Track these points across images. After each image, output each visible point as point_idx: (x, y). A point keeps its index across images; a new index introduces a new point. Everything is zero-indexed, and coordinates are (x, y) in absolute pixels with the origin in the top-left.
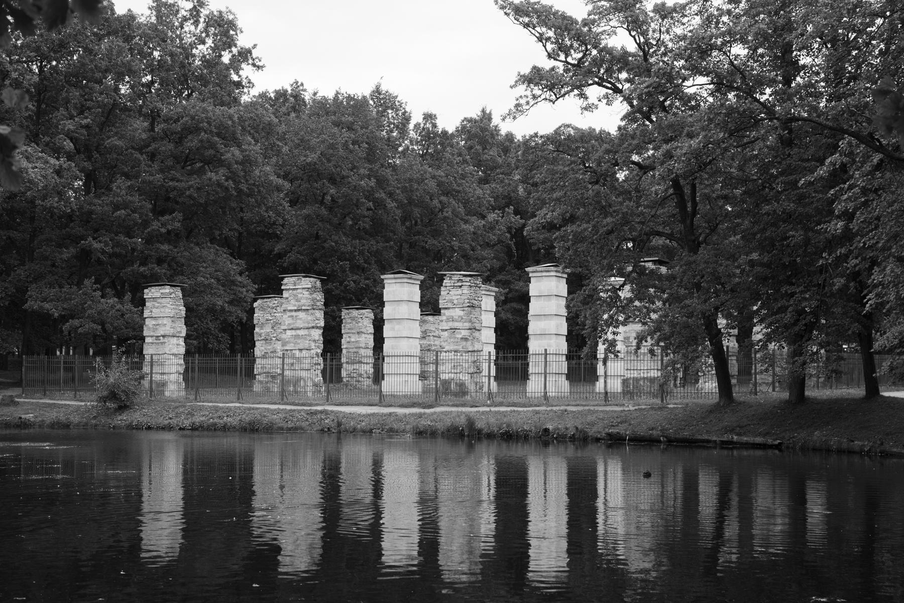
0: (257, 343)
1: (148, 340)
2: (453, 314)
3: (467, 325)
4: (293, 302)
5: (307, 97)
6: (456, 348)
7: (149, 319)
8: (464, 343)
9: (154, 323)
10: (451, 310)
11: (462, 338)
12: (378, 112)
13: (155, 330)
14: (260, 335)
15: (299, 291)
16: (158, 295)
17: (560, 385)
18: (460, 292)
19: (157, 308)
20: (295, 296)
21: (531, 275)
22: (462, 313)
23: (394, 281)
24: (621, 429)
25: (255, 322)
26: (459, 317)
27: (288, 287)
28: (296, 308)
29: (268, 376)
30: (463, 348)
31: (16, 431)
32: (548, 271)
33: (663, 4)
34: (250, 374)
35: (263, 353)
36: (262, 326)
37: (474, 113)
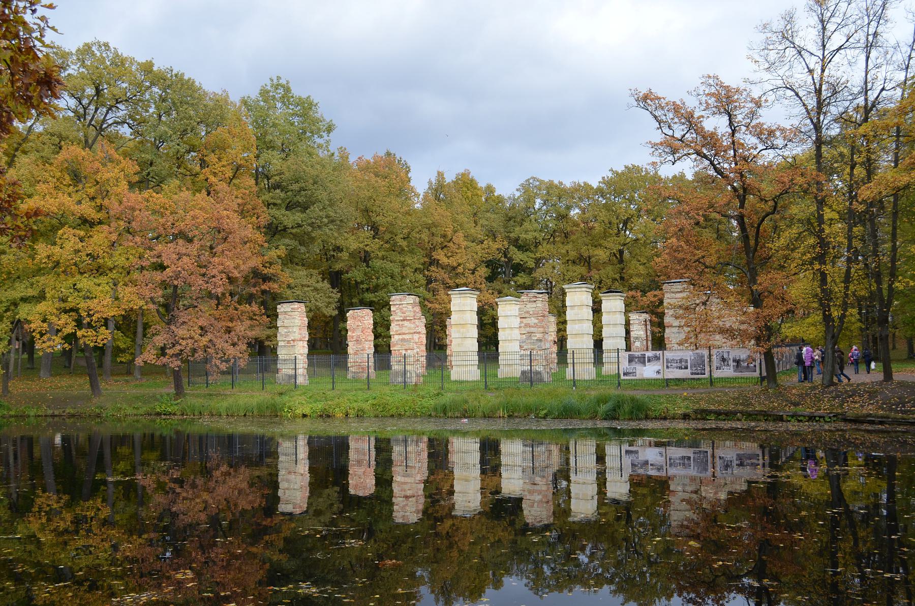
3: (541, 330)
4: (400, 314)
5: (352, 159)
13: (286, 336)
14: (352, 337)
16: (289, 310)
18: (534, 305)
22: (536, 321)
23: (459, 296)
31: (722, 424)
33: (183, 74)
37: (462, 171)
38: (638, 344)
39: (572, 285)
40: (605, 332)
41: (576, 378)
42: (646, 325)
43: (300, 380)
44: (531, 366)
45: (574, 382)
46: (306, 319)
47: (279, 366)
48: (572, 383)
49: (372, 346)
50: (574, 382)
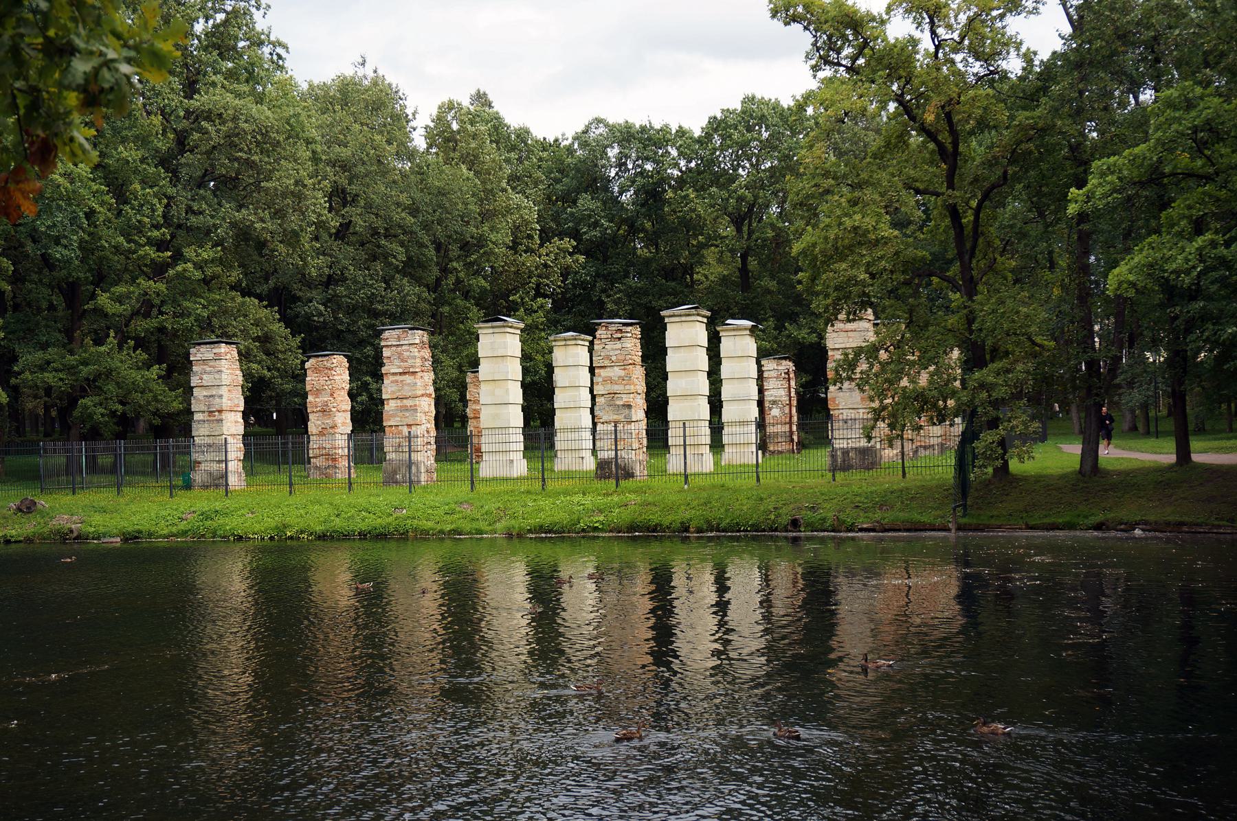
0: (311, 416)
1: (197, 417)
2: (611, 374)
4: (397, 362)
6: (615, 417)
7: (199, 389)
8: (627, 411)
9: (205, 394)
10: (609, 369)
11: (623, 405)
12: (923, 211)
15: (404, 347)
16: (211, 356)
17: (707, 462)
18: (619, 345)
19: (209, 373)
20: (400, 354)
21: (666, 320)
23: (491, 331)
24: (655, 517)
25: (308, 388)
26: (619, 377)
27: (390, 343)
28: (401, 371)
29: (328, 459)
30: (625, 417)
32: (689, 315)
34: (302, 458)
35: (320, 429)
36: (318, 392)
38: (775, 412)
39: (676, 310)
40: (726, 392)
41: (688, 471)
42: (789, 380)
43: (233, 480)
44: (616, 450)
45: (686, 477)
46: (239, 373)
47: (195, 456)
48: (683, 479)
49: (349, 421)
50: (686, 477)
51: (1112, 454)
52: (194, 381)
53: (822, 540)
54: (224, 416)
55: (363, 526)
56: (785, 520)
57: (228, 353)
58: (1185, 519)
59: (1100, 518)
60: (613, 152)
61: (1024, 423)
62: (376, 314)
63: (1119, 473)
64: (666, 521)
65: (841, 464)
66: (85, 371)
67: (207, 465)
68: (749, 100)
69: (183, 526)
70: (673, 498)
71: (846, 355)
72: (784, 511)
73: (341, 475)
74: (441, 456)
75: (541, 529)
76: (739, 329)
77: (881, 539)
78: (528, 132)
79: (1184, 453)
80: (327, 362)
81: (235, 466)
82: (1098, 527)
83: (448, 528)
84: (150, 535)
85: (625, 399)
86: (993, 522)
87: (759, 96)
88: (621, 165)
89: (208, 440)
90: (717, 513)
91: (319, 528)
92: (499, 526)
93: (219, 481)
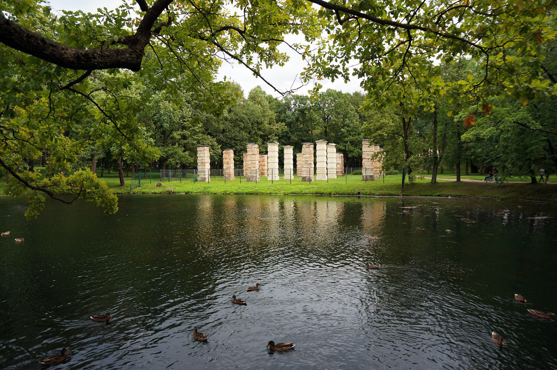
1: (198, 164)
4: (251, 152)
16: (202, 149)
18: (308, 149)
36: (226, 159)
39: (319, 141)
51: (440, 179)
52: (198, 155)
53: (366, 197)
54: (206, 164)
55: (247, 191)
56: (356, 192)
57: (207, 149)
58: (462, 194)
59: (439, 194)
60: (292, 102)
61: (422, 171)
62: (236, 140)
63: (442, 183)
64: (325, 192)
65: (366, 179)
66: (170, 152)
67: (201, 176)
68: (329, 89)
69: (200, 190)
70: (326, 186)
71: (375, 153)
72: (356, 190)
73: (207, 180)
74: (211, 175)
75: (293, 193)
76: (332, 146)
77: (382, 197)
78: (272, 96)
79: (458, 179)
80: (228, 151)
81: (207, 176)
82: (438, 196)
83: (269, 192)
84: (191, 192)
85: (310, 162)
86: (411, 194)
87: (343, 92)
88: (295, 105)
89: (201, 170)
90: (338, 190)
91: (235, 192)
92: (281, 192)
93: (204, 180)
